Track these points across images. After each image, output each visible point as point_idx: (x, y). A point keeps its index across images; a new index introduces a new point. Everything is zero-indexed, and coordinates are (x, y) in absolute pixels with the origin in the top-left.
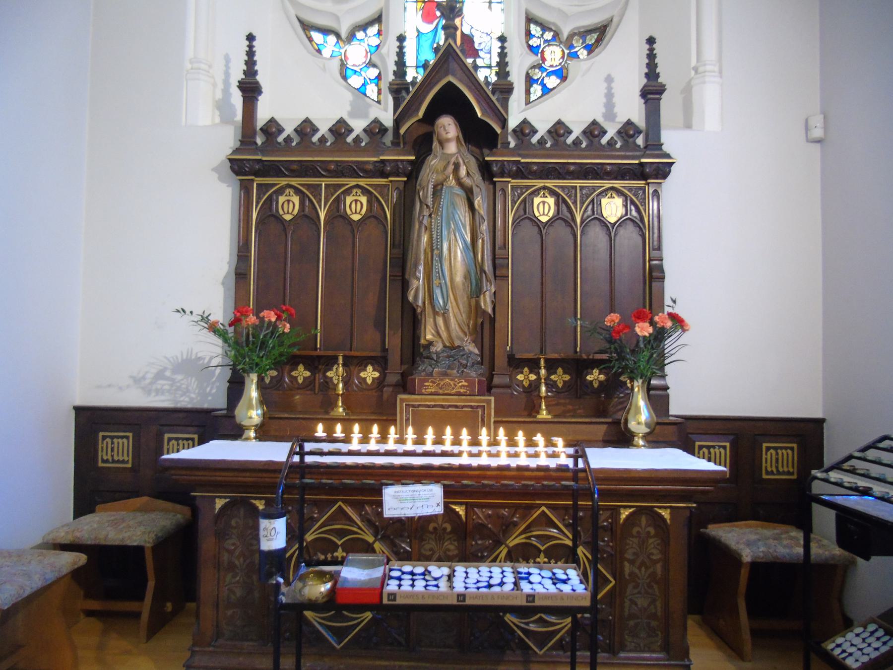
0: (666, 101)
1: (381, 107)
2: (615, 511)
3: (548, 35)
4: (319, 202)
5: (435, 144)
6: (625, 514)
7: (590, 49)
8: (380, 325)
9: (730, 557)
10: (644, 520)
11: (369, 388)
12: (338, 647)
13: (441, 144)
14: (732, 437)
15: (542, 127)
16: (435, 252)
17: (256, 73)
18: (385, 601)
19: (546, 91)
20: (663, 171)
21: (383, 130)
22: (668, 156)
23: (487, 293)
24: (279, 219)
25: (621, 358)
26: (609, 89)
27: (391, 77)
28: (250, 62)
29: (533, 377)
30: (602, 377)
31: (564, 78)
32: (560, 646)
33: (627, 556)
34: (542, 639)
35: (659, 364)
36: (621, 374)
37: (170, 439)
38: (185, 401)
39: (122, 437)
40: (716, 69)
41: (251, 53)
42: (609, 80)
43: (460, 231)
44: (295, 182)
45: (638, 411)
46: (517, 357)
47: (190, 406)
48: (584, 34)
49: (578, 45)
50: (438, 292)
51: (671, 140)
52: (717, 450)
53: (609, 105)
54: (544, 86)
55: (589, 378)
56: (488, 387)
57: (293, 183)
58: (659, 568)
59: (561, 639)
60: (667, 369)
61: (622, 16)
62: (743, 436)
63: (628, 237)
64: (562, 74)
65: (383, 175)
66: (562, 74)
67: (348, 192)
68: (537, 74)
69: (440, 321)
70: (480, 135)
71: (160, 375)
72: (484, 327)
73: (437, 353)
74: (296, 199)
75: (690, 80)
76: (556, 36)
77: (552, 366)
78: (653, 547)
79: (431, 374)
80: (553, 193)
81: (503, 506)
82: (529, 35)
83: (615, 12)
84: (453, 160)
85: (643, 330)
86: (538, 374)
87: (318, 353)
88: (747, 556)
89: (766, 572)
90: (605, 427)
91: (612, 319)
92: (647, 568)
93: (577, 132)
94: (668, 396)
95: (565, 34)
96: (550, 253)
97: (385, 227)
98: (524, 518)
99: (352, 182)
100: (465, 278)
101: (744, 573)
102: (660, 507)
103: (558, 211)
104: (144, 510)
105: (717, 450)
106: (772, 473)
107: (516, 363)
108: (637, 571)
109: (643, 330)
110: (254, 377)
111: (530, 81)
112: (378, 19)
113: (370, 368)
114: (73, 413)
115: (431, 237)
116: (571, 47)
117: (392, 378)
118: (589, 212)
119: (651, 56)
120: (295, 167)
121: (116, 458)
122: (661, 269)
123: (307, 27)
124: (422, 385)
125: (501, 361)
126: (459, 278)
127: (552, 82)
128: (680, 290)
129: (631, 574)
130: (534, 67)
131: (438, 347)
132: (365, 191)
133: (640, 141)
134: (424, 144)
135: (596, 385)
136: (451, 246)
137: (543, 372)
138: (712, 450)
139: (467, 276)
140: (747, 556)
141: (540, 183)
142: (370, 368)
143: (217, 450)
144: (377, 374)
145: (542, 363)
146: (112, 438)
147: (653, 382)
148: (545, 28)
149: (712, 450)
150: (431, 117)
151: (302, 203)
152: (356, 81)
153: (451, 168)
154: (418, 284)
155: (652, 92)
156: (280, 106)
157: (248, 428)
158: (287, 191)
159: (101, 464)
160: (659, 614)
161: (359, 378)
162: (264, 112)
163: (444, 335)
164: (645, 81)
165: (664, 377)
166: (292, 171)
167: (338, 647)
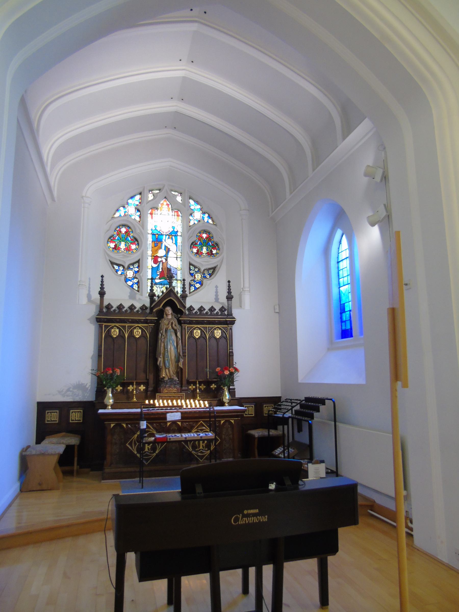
1: (140, 293)
2: (220, 421)
3: (196, 270)
4: (125, 331)
5: (165, 315)
6: (222, 422)
7: (210, 275)
8: (145, 372)
9: (252, 436)
10: (227, 423)
11: (142, 392)
12: (146, 464)
13: (167, 315)
14: (254, 404)
15: (196, 307)
17: (104, 288)
18: (168, 440)
20: (233, 323)
21: (146, 308)
22: (234, 318)
24: (111, 337)
25: (221, 380)
26: (217, 290)
27: (149, 291)
28: (102, 285)
29: (194, 387)
30: (215, 386)
31: (202, 285)
32: (207, 459)
34: (202, 457)
35: (232, 382)
36: (221, 385)
37: (72, 412)
38: (77, 399)
39: (55, 412)
40: (248, 290)
41: (102, 282)
42: (217, 287)
44: (117, 325)
45: (226, 396)
46: (190, 381)
47: (79, 400)
49: (206, 273)
50: (166, 362)
51: (236, 313)
53: (217, 299)
54: (195, 287)
55: (211, 387)
56: (182, 391)
58: (231, 436)
59: (207, 457)
60: (235, 383)
62: (258, 402)
63: (223, 341)
64: (201, 283)
65: (147, 323)
66: (201, 283)
67: (135, 328)
68: (193, 283)
69: (167, 370)
70: (177, 311)
71: (68, 390)
72: (180, 372)
73: (167, 381)
74: (117, 330)
75: (241, 292)
76: (199, 270)
77: (200, 383)
79: (165, 387)
80: (200, 329)
82: (190, 270)
83: (219, 264)
84: (171, 322)
85: (227, 373)
86: (196, 386)
87: (125, 381)
88: (257, 435)
89: (261, 439)
90: (217, 401)
91: (218, 369)
93: (207, 310)
94: (235, 392)
96: (199, 347)
97: (147, 339)
98: (196, 424)
99: (136, 325)
101: (256, 441)
103: (201, 334)
104: (63, 436)
107: (189, 383)
109: (227, 373)
110: (110, 389)
111: (190, 285)
113: (142, 386)
115: (164, 345)
116: (204, 274)
117: (150, 389)
118: (211, 335)
119: (229, 286)
120: (118, 320)
121: (52, 420)
122: (232, 352)
123: (112, 263)
124: (163, 390)
125: (184, 382)
126: (173, 357)
127: (198, 286)
128: (239, 359)
130: (191, 280)
131: (166, 379)
132: (140, 328)
133: (226, 313)
135: (213, 389)
136: (170, 346)
137: (198, 385)
139: (175, 357)
140: (257, 435)
141: (196, 326)
142: (142, 386)
144: (144, 388)
145: (198, 382)
147: (231, 387)
150: (165, 306)
151: (119, 332)
152: (130, 283)
153: (170, 324)
154: (160, 359)
155: (230, 297)
157: (108, 406)
158: (114, 328)
163: (168, 374)
164: (227, 294)
165: (234, 386)
167: (146, 464)
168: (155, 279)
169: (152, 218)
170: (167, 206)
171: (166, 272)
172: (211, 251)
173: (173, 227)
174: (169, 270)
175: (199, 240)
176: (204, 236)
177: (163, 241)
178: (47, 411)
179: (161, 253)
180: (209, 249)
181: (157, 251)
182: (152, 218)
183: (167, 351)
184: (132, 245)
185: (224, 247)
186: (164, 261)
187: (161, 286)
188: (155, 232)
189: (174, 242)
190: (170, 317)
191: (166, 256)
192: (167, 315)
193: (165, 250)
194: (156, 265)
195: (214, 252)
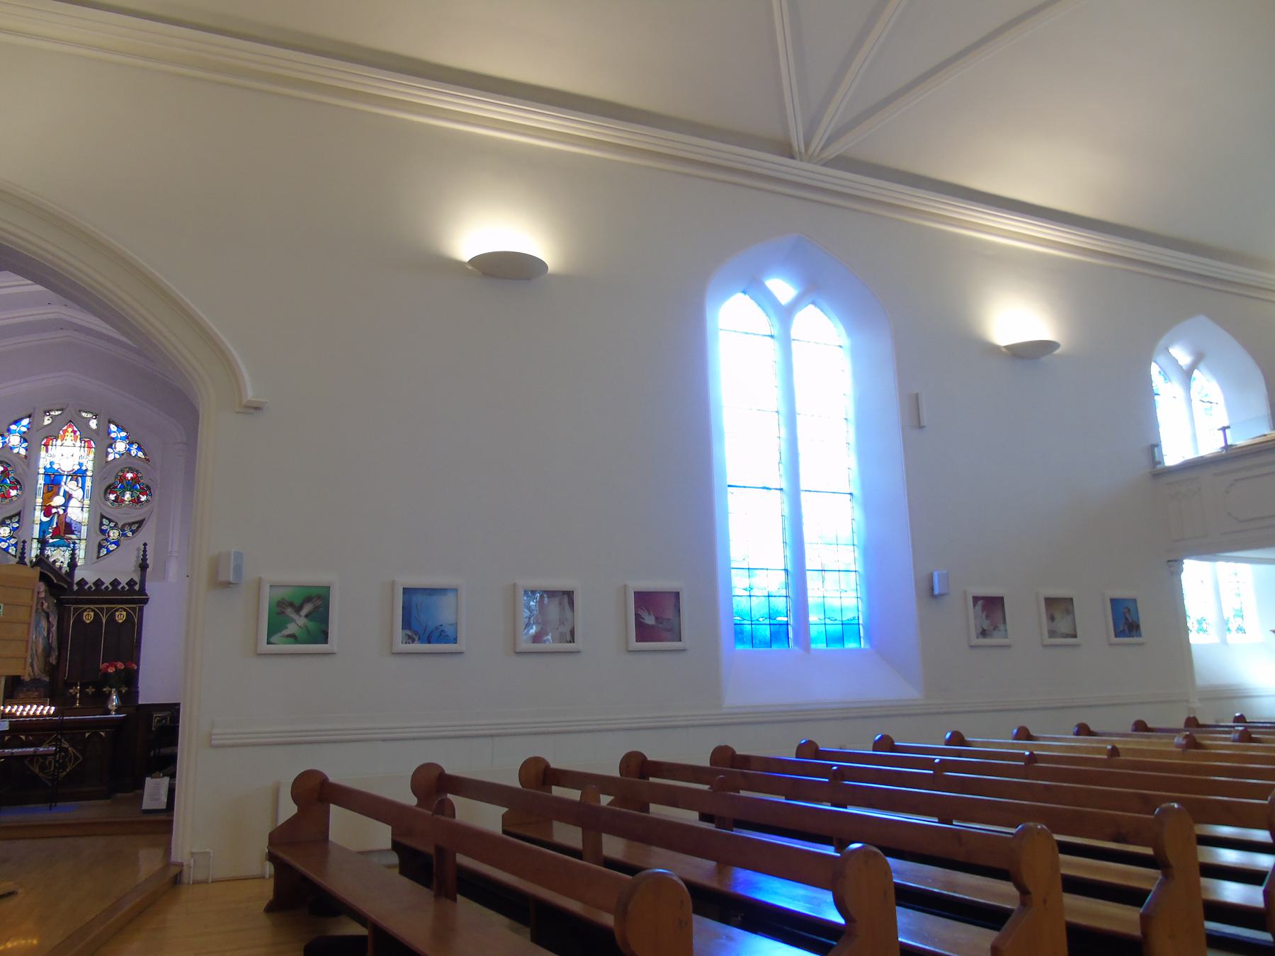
3: (112, 525)
7: (133, 532)
19: (109, 552)
20: (146, 601)
48: (130, 524)
51: (151, 588)
64: (117, 543)
68: (105, 544)
82: (101, 524)
112: (19, 514)
127: (112, 547)
148: (110, 521)
155: (143, 566)
171: (62, 528)
179: (58, 500)
181: (51, 498)
186: (61, 512)
191: (65, 506)
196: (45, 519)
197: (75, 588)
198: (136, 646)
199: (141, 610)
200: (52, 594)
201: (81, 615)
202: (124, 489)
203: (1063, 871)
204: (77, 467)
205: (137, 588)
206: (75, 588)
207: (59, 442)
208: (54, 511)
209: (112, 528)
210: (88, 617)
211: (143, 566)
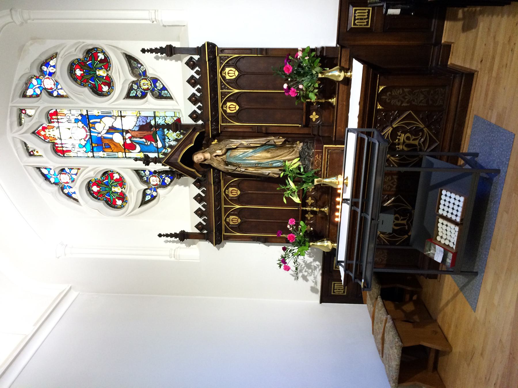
0: (176, 44)
3: (135, 87)
5: (206, 163)
6: (379, 107)
13: (205, 160)
16: (256, 165)
20: (212, 46)
23: (275, 141)
28: (171, 235)
33: (399, 105)
41: (167, 235)
43: (247, 155)
50: (274, 165)
51: (196, 41)
52: (357, 15)
57: (224, 218)
58: (406, 90)
61: (122, 49)
67: (224, 78)
68: (156, 92)
78: (397, 92)
81: (376, 118)
83: (119, 52)
92: (406, 95)
95: (135, 79)
100: (268, 152)
102: (378, 90)
105: (357, 15)
106: (368, 22)
108: (407, 100)
114: (323, 304)
120: (217, 219)
126: (269, 155)
129: (408, 102)
130: (153, 95)
134: (205, 167)
138: (356, 18)
139: (268, 151)
143: (342, 256)
146: (334, 289)
149: (356, 18)
151: (230, 101)
155: (170, 51)
156: (190, 223)
159: (345, 294)
160: (427, 89)
161: (312, 192)
162: (191, 229)
166: (219, 219)
168: (157, 148)
169: (69, 151)
170: (47, 130)
171: (146, 133)
172: (101, 61)
173: (77, 121)
174: (142, 128)
175: (86, 81)
176: (78, 72)
177: (100, 135)
178: (332, 293)
179: (118, 138)
180: (99, 66)
181: (116, 145)
182: (69, 151)
183: (258, 164)
184: (115, 178)
185: (91, 43)
186: (129, 135)
187: (167, 140)
188: (89, 146)
189: (99, 120)
190: (208, 155)
191: (122, 132)
192: (205, 160)
193: (112, 134)
194: (137, 146)
195: (101, 56)
196: (138, 148)
197: (200, 122)
198: (265, 53)
199: (222, 50)
200: (208, 145)
201: (230, 116)
202: (95, 77)
203: (439, 275)
204: (80, 124)
205: (196, 57)
206: (200, 122)
207: (58, 141)
208: (128, 141)
209: (139, 87)
210: (232, 107)
211: (170, 51)
